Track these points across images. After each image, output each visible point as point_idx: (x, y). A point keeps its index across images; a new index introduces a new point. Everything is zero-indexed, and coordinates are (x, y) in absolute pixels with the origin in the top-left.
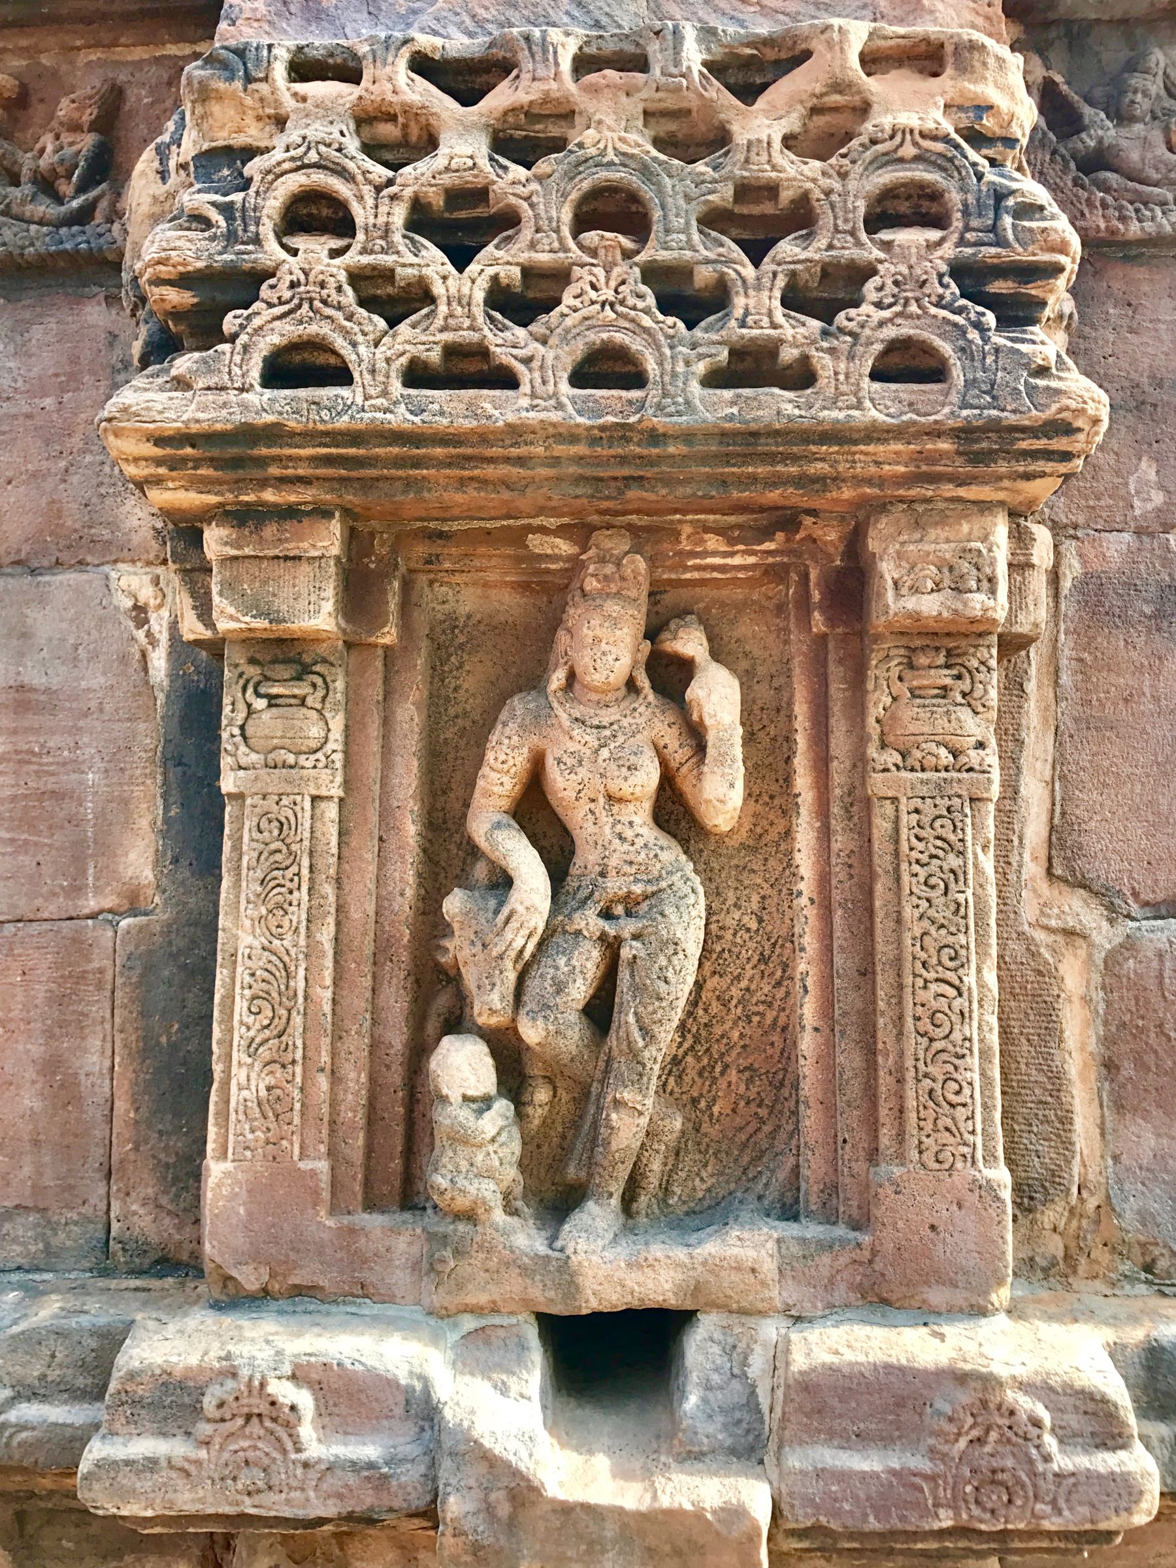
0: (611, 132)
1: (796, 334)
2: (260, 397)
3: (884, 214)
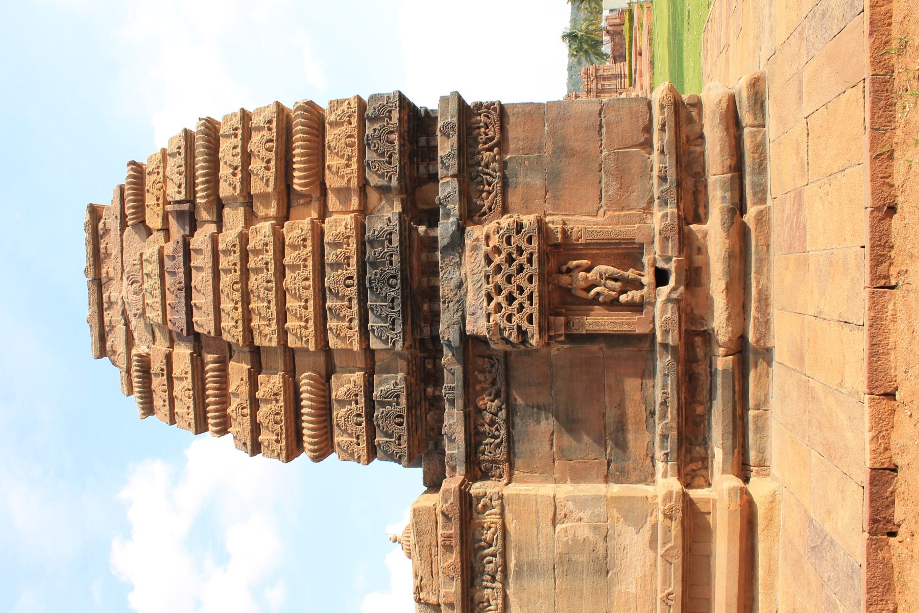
0: (499, 279)
1: (525, 255)
2: (534, 325)
3: (509, 243)
